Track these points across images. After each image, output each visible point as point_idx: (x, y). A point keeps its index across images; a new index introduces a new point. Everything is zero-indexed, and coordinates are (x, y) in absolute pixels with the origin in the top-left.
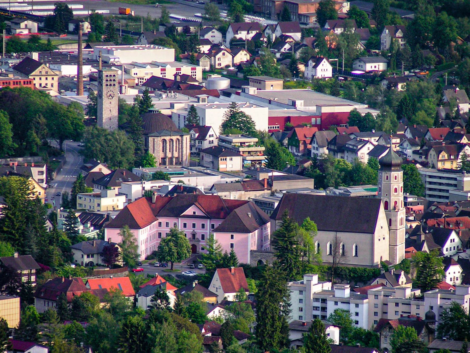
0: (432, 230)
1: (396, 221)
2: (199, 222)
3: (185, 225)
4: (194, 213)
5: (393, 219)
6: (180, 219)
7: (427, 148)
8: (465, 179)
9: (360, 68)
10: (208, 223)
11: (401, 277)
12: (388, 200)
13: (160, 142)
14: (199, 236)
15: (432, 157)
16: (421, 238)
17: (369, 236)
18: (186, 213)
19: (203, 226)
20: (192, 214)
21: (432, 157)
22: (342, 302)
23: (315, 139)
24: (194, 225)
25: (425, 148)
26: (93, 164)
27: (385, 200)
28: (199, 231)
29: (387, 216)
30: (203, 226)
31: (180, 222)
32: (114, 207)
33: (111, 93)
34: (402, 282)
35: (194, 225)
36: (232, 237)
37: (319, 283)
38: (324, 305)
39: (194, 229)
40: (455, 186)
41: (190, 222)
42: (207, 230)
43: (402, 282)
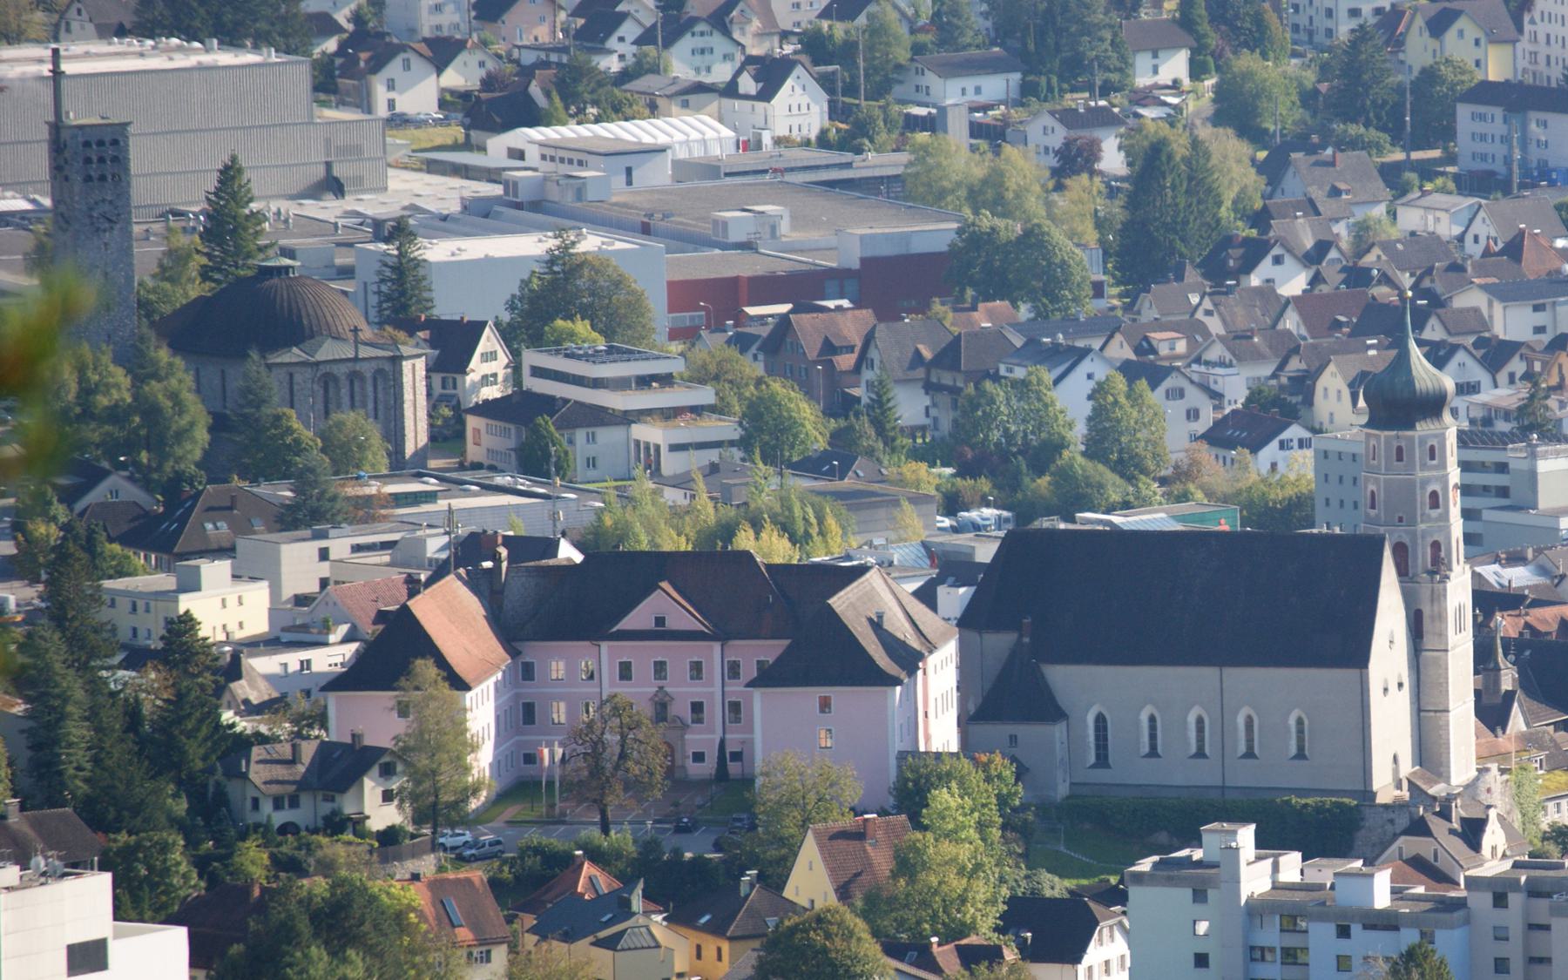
0: (1527, 653)
1: (1441, 617)
2: (678, 656)
3: (625, 672)
4: (660, 621)
5: (1426, 610)
6: (605, 645)
7: (1303, 366)
8: (1543, 466)
9: (921, 97)
10: (713, 655)
11: (1489, 829)
12: (1406, 540)
13: (316, 387)
14: (681, 709)
15: (1332, 394)
16: (1497, 682)
17: (1351, 674)
18: (629, 622)
19: (697, 669)
20: (650, 624)
21: (1332, 394)
22: (1365, 927)
23: (873, 354)
24: (660, 668)
25: (1295, 365)
26: (1322, 297)
27: (1396, 539)
28: (683, 691)
29: (1409, 598)
30: (697, 669)
31: (608, 654)
32: (229, 629)
33: (107, 207)
34: (1494, 849)
35: (660, 668)
36: (825, 705)
37: (1259, 858)
38: (1291, 941)
39: (660, 683)
40: (1503, 492)
41: (643, 655)
42: (712, 685)
43: (1494, 849)
